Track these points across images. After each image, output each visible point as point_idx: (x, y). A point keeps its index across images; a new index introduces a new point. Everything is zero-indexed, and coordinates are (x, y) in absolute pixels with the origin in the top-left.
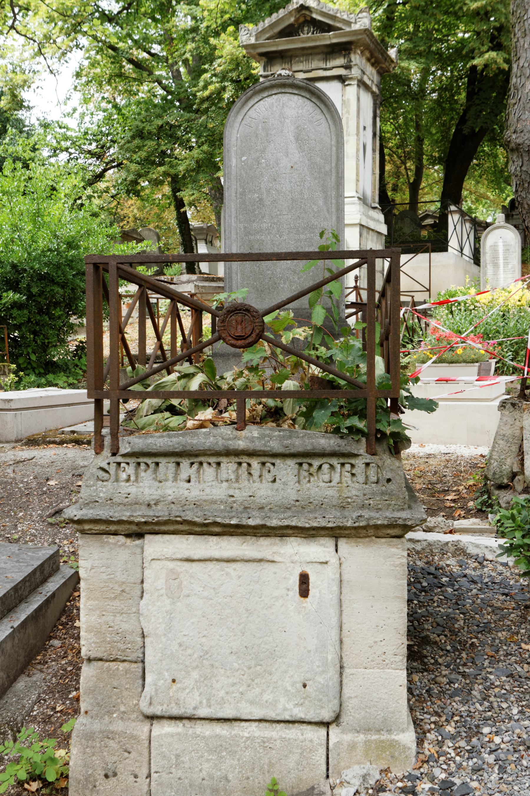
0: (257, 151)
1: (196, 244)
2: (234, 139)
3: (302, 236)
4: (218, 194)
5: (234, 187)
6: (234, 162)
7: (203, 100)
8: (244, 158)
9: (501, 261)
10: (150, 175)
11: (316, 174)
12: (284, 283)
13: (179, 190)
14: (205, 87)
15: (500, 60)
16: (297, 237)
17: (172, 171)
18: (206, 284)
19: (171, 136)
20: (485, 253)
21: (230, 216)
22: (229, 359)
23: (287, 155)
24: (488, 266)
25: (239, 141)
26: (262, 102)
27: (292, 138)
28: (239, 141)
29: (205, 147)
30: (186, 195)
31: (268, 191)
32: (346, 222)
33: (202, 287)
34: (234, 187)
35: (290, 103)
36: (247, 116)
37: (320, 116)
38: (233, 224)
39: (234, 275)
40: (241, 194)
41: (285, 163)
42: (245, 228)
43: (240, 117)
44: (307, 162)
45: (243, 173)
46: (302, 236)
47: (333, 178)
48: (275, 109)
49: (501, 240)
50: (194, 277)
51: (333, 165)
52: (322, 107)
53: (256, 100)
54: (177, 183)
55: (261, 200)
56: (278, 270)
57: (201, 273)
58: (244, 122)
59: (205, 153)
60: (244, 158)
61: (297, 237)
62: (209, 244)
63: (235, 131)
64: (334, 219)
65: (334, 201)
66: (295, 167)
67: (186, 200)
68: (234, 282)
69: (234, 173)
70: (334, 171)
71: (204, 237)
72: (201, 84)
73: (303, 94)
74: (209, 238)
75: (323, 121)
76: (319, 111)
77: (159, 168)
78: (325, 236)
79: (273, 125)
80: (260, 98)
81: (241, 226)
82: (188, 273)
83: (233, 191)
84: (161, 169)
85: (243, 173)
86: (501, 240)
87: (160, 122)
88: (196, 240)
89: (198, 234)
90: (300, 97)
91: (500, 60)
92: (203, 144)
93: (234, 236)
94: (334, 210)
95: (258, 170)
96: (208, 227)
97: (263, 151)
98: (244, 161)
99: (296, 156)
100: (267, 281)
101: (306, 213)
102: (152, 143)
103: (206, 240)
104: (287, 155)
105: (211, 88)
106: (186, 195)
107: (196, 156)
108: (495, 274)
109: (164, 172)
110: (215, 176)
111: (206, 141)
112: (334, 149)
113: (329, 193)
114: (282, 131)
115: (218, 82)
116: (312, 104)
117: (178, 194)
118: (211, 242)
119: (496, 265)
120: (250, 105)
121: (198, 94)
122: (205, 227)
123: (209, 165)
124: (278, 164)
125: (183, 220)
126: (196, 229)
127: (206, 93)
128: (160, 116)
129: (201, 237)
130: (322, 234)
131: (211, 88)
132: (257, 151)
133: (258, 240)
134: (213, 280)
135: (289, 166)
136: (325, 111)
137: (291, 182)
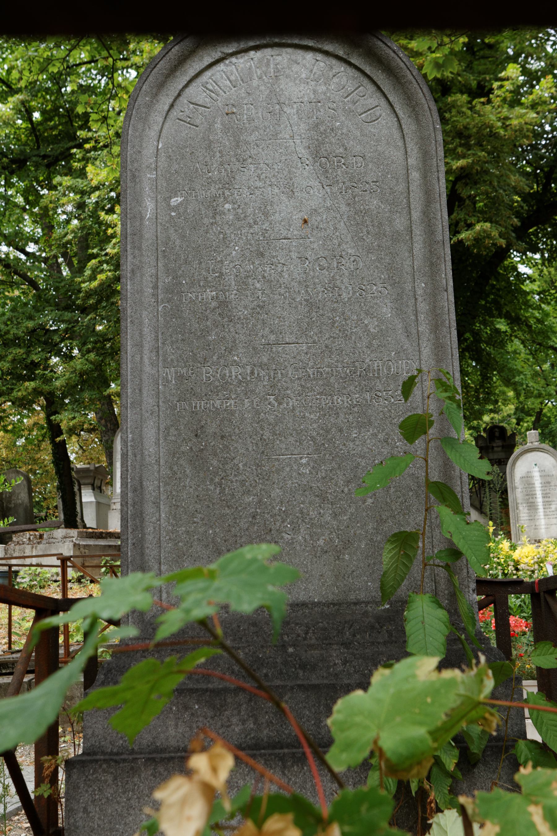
0: (210, 182)
1: (80, 490)
2: (148, 151)
3: (339, 400)
4: (110, 425)
5: (149, 271)
6: (149, 207)
7: (89, 294)
8: (176, 201)
9: (540, 500)
10: (15, 394)
11: (369, 239)
12: (295, 530)
13: (56, 413)
14: (93, 278)
15: (495, 234)
16: (325, 401)
17: (46, 388)
18: (91, 542)
19: (46, 343)
20: (514, 488)
21: (139, 346)
22: (134, 771)
23: (291, 194)
24: (521, 508)
25: (163, 158)
26: (221, 67)
27: (302, 152)
28: (163, 158)
29: (92, 356)
30: (64, 419)
31: (243, 283)
32: (13, 606)
33: (85, 546)
34: (149, 271)
35: (295, 68)
36: (183, 100)
37: (372, 99)
38: (148, 368)
39: (149, 509)
40: (168, 290)
41: (286, 211)
42: (180, 378)
43: (165, 101)
44: (344, 208)
45: (174, 236)
46: (339, 400)
47: (418, 246)
48: (255, 83)
49: (536, 469)
50: (74, 532)
51: (416, 215)
52: (380, 77)
53: (208, 60)
54: (53, 406)
55: (224, 304)
56: (276, 492)
57: (85, 527)
58: (174, 113)
59: (91, 363)
60: (176, 201)
61: (325, 401)
62: (97, 491)
63: (153, 133)
64: (426, 351)
65: (423, 306)
66: (313, 221)
67: (63, 426)
68: (150, 529)
69: (148, 234)
70: (418, 231)
71: (90, 481)
72: (88, 273)
73: (329, 47)
74: (97, 483)
75: (383, 111)
76: (371, 88)
77: (27, 384)
78: (416, 391)
79: (251, 120)
80: (217, 55)
81: (171, 373)
82: (66, 527)
83: (147, 281)
84: (31, 385)
85: (174, 236)
86: (536, 469)
87: (30, 324)
88: (80, 485)
89: (84, 477)
90: (319, 56)
91: (495, 234)
92: (89, 351)
93: (149, 401)
94: (424, 328)
95: (216, 229)
96: (96, 468)
97: (228, 183)
98: (175, 208)
99: (313, 192)
100: (243, 524)
101: (347, 337)
102: (18, 350)
103: (93, 485)
104: (291, 193)
105: (101, 277)
106: (64, 419)
107: (79, 367)
108: (533, 518)
109: (35, 389)
110: (105, 393)
111: (94, 348)
112: (415, 175)
113: (408, 287)
114: (275, 135)
115: (110, 271)
116: (351, 72)
117: (53, 418)
118: (100, 488)
119: (532, 506)
120: (191, 72)
121: (83, 285)
122: (92, 468)
123: (95, 381)
124: (266, 214)
125: (60, 453)
126: (79, 471)
127: (95, 284)
128: (31, 318)
129: (87, 481)
130: (408, 387)
131: (101, 277)
132: (210, 182)
133: (217, 412)
134: (100, 536)
135: (297, 217)
136: (386, 86)
137: (303, 259)
